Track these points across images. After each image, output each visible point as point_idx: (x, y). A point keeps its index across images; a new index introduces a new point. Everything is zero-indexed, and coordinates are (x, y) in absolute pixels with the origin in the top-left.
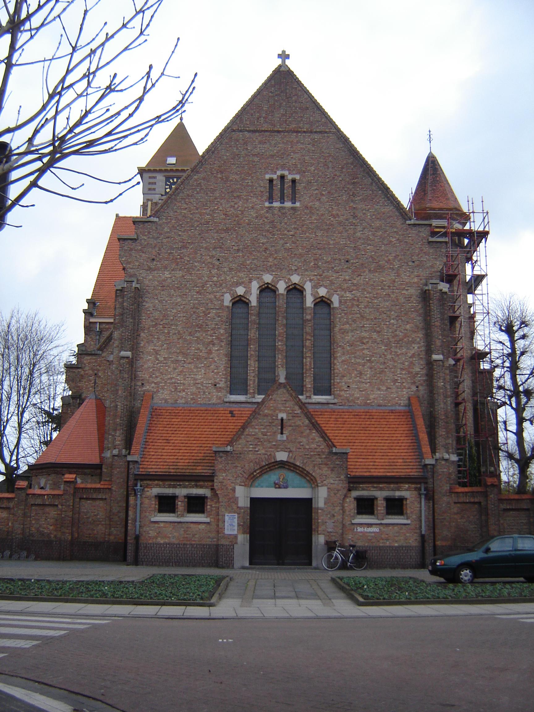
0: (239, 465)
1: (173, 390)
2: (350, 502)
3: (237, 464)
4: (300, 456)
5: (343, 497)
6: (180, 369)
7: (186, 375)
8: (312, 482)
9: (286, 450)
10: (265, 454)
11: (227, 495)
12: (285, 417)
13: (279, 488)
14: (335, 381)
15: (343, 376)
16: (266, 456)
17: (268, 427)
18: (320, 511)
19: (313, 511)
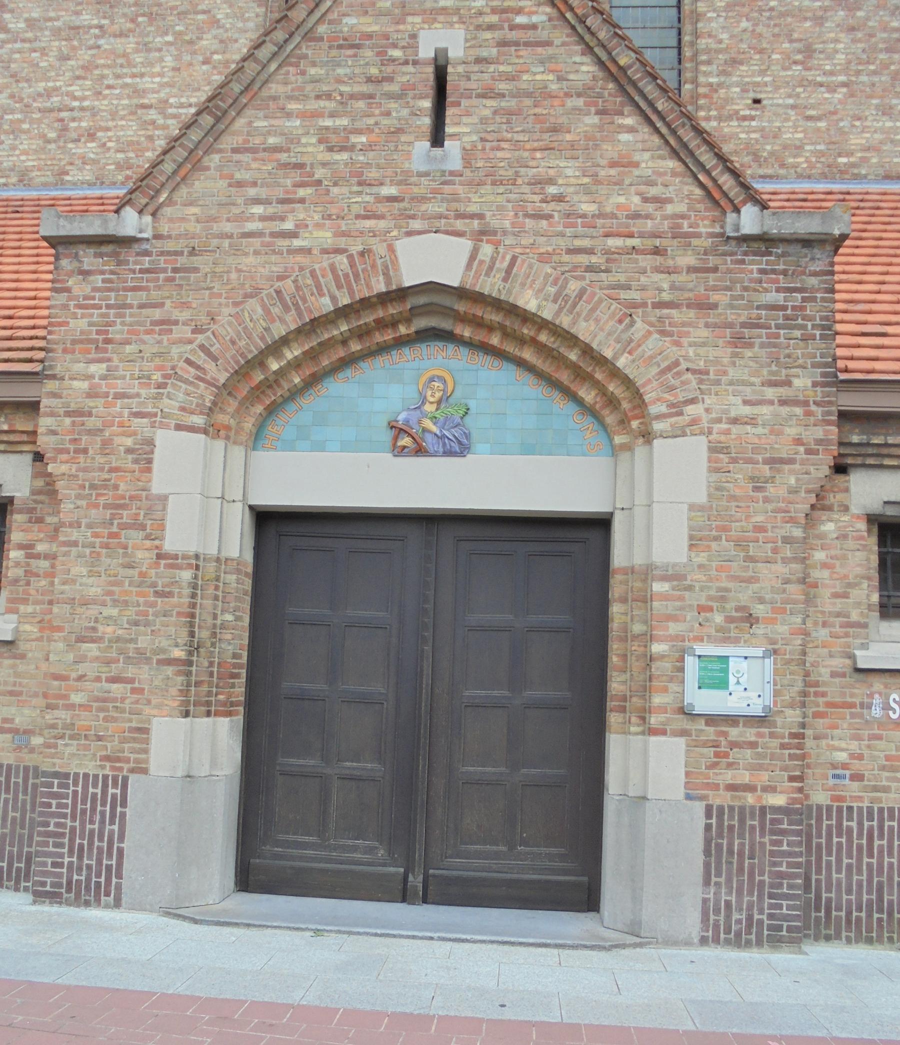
0: (184, 315)
1: (52, 135)
2: (843, 537)
3: (169, 310)
4: (544, 258)
5: (802, 508)
6: (85, 55)
7: (103, 77)
8: (611, 419)
9: (459, 225)
10: (338, 251)
11: (106, 484)
12: (456, 52)
13: (420, 451)
14: (702, 79)
15: (735, 62)
16: (342, 261)
17: (361, 104)
18: (658, 587)
19: (616, 589)
